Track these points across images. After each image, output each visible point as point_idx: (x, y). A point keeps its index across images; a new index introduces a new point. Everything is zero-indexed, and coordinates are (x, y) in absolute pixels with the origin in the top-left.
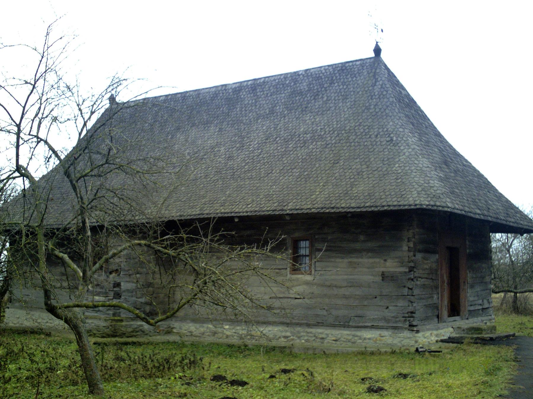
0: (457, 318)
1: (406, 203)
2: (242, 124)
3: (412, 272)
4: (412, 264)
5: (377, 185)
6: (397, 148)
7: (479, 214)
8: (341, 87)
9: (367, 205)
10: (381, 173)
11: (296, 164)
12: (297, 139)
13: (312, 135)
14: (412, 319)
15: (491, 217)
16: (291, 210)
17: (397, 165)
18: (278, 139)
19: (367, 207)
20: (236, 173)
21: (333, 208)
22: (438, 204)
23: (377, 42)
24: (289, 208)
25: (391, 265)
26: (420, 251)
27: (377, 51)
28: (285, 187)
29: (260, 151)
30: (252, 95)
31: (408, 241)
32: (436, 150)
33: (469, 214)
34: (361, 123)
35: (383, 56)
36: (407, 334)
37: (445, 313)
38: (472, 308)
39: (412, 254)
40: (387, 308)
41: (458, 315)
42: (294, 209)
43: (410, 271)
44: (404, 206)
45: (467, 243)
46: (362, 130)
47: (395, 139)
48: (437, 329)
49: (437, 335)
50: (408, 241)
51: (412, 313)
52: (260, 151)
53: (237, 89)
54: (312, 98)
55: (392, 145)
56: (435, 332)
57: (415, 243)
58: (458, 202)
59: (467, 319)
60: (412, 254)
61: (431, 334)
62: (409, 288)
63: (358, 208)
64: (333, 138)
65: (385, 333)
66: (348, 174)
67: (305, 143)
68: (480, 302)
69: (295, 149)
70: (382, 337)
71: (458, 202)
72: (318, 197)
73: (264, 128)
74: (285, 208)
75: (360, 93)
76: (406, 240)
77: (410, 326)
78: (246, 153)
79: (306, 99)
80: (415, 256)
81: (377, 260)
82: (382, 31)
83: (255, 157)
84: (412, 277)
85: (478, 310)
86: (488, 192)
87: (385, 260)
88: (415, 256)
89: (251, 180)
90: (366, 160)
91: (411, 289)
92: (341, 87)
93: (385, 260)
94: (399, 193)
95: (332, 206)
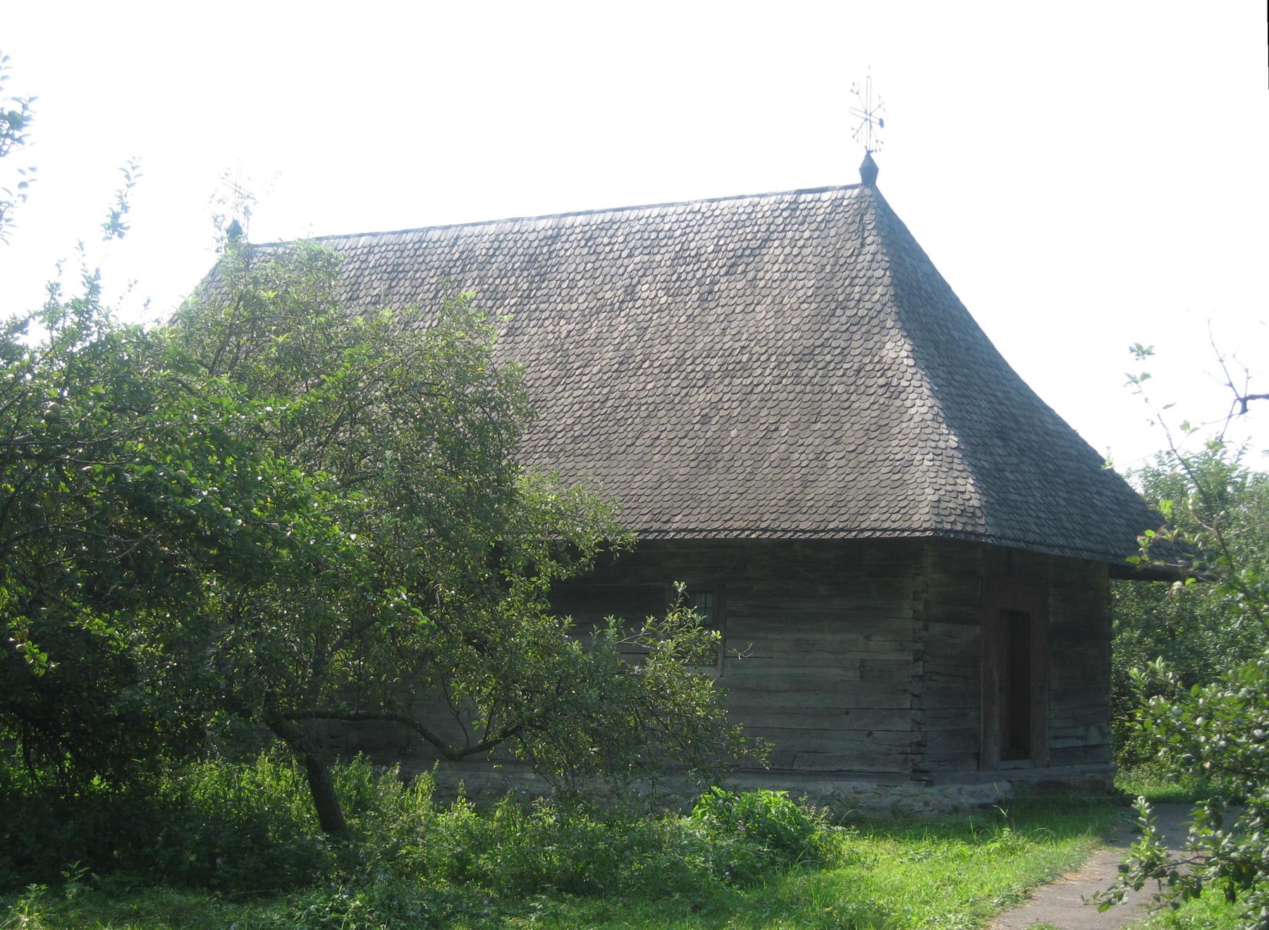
0: (1024, 763)
1: (906, 525)
2: (563, 322)
3: (921, 663)
4: (920, 646)
5: (853, 483)
7: (1060, 547)
8: (787, 250)
9: (831, 526)
11: (688, 427)
12: (691, 368)
13: (721, 361)
14: (919, 757)
15: (1091, 551)
16: (678, 531)
17: (896, 442)
18: (646, 365)
19: (832, 530)
20: (554, 441)
21: (765, 530)
23: (869, 152)
24: (674, 526)
25: (880, 648)
27: (869, 171)
28: (663, 479)
29: (605, 391)
30: (586, 250)
31: (915, 599)
32: (984, 404)
33: (1036, 548)
34: (827, 339)
35: (881, 183)
36: (909, 787)
37: (994, 752)
38: (1058, 744)
39: (920, 624)
40: (870, 734)
41: (1026, 756)
42: (684, 530)
43: (916, 660)
44: (903, 530)
45: (1051, 601)
46: (828, 358)
48: (977, 781)
49: (972, 794)
50: (915, 599)
51: (919, 744)
52: (605, 391)
53: (550, 232)
54: (723, 271)
55: (888, 395)
56: (969, 788)
58: (1014, 524)
59: (1048, 766)
60: (920, 624)
61: (960, 790)
62: (913, 695)
63: (815, 531)
64: (768, 371)
65: (864, 785)
66: (796, 455)
67: (707, 378)
68: (1081, 731)
69: (685, 391)
70: (859, 793)
71: (1014, 524)
72: (647, 203)
73: (615, 334)
74: (666, 527)
75: (828, 268)
76: (911, 596)
77: (914, 771)
78: (577, 393)
79: (709, 271)
80: (926, 629)
82: (881, 123)
83: (597, 405)
84: (921, 673)
85: (1076, 748)
86: (1098, 493)
87: (868, 637)
88: (926, 629)
89: (590, 458)
90: (836, 427)
91: (918, 696)
92: (787, 250)
94: (895, 503)
95: (763, 525)
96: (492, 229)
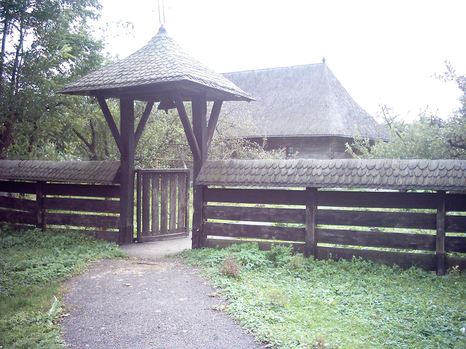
6: (328, 109)
9: (315, 134)
10: (321, 120)
22: (340, 134)
26: (336, 151)
27: (324, 60)
29: (272, 107)
35: (326, 62)
47: (328, 105)
57: (334, 148)
74: (283, 134)
81: (319, 155)
87: (322, 155)
93: (322, 155)
96: (247, 72)
